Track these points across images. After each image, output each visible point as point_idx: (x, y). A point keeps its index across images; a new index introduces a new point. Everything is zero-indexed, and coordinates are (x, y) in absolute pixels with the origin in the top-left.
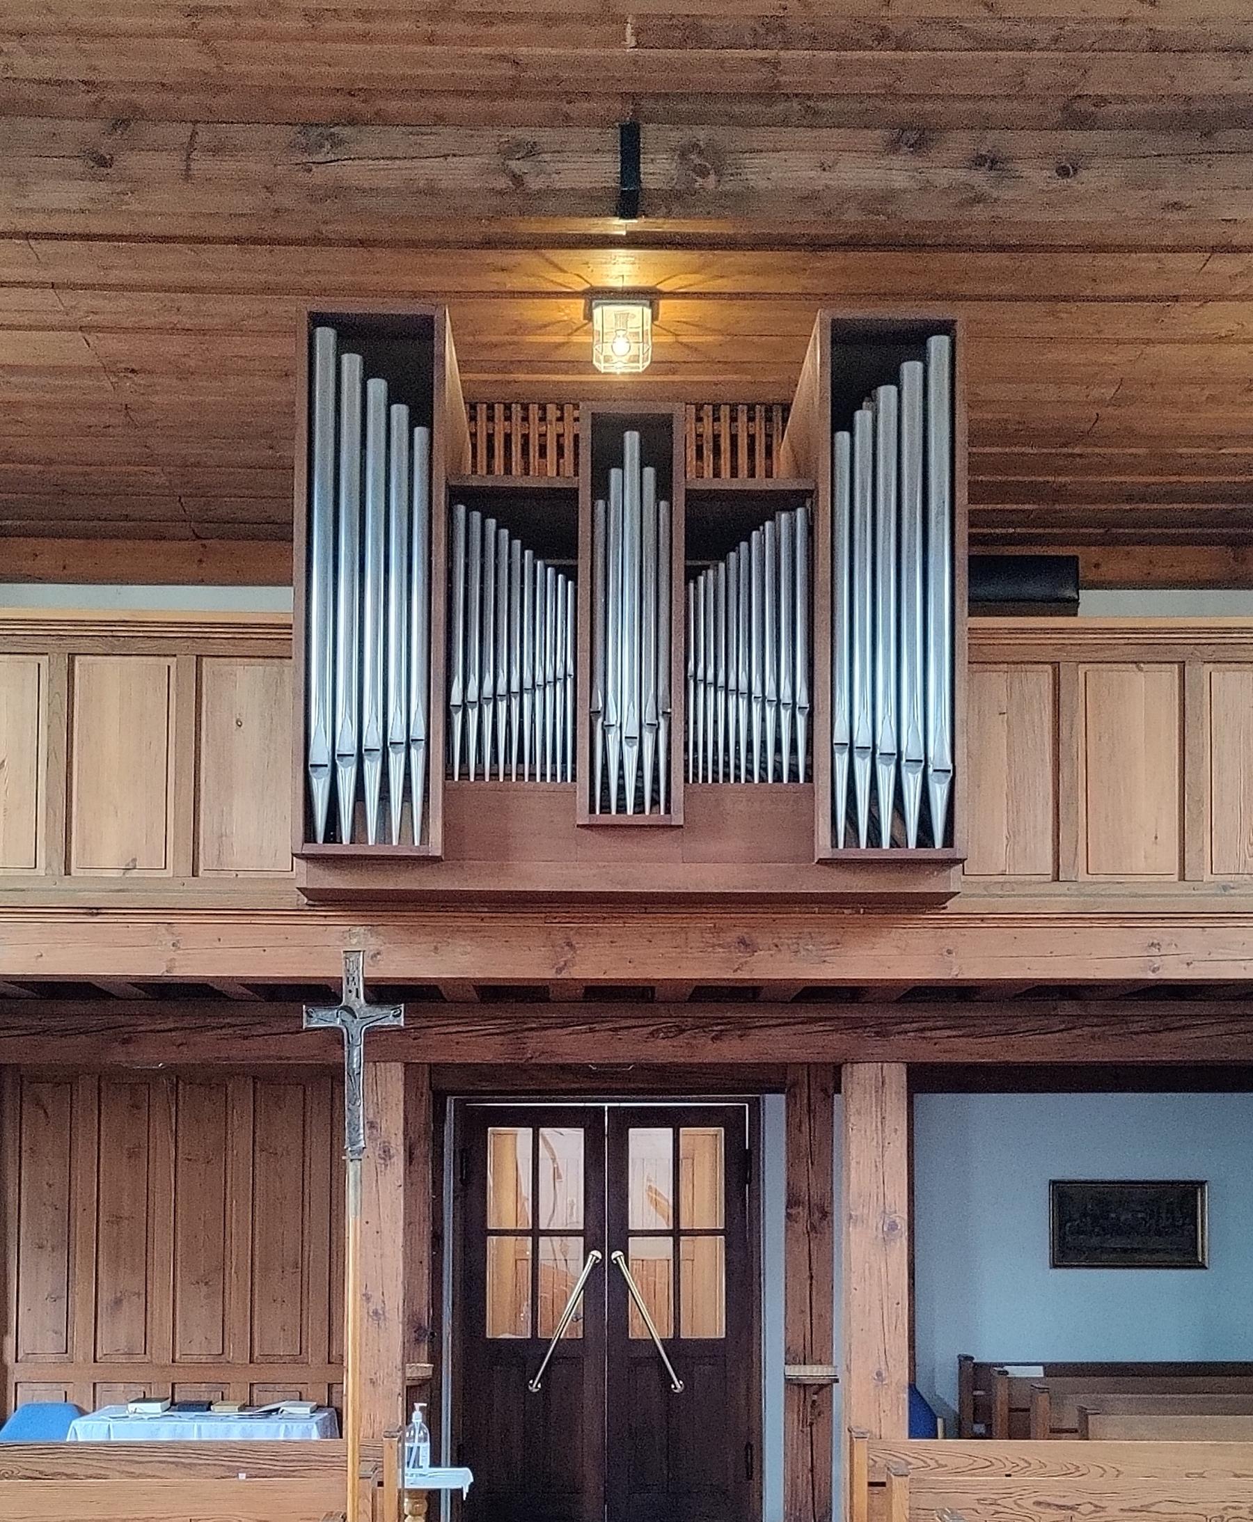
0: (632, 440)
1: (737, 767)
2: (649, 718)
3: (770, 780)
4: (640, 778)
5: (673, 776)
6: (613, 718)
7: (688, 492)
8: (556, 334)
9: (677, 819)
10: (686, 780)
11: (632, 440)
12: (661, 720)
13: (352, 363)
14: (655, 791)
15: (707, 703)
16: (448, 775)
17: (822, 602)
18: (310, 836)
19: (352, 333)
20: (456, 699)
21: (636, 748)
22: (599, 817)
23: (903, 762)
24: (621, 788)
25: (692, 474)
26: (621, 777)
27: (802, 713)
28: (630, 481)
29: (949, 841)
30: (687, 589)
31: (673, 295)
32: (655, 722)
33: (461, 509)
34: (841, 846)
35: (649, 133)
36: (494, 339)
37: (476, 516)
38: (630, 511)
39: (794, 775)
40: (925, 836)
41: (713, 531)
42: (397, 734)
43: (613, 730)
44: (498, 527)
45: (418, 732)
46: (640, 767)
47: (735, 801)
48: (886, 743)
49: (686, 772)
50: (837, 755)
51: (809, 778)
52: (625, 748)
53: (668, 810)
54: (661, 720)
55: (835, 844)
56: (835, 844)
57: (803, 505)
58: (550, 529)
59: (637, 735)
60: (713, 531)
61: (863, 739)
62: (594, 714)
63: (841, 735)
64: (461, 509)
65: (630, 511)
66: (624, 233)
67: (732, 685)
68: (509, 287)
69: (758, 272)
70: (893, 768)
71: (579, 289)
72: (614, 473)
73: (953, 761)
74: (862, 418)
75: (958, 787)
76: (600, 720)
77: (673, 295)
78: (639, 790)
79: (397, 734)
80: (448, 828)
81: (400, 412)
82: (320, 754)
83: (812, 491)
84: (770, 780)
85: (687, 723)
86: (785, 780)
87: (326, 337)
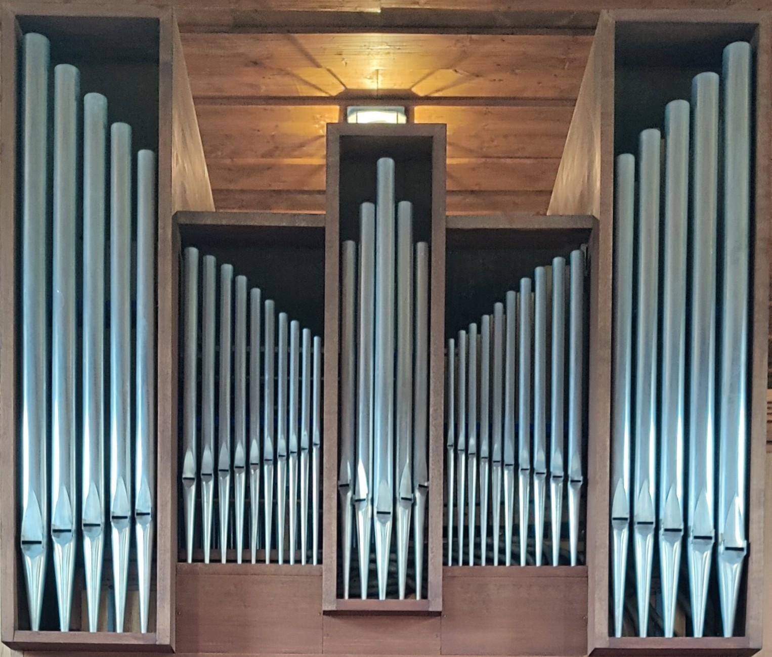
0: (386, 167)
1: (502, 551)
2: (403, 492)
3: (538, 563)
4: (393, 561)
5: (430, 555)
6: (363, 491)
7: (449, 231)
8: (311, 156)
9: (435, 605)
10: (445, 563)
11: (386, 167)
12: (418, 494)
13: (67, 74)
14: (410, 576)
15: (466, 472)
16: (181, 558)
17: (601, 352)
18: (23, 620)
19: (71, 43)
20: (189, 471)
21: (389, 524)
22: (347, 603)
23: (691, 539)
24: (373, 574)
25: (454, 213)
26: (373, 561)
27: (574, 487)
28: (384, 218)
29: (740, 628)
30: (447, 345)
31: (428, 100)
32: (410, 496)
33: (193, 252)
34: (618, 633)
35: (447, 189)
36: (251, 161)
37: (210, 260)
38: (384, 272)
39: (564, 559)
40: (713, 624)
41: (478, 275)
42: (120, 506)
43: (363, 504)
44: (236, 274)
45: (144, 503)
46: (393, 549)
47: (499, 586)
48: (671, 517)
49: (445, 555)
50: (615, 532)
51: (581, 561)
52: (378, 525)
53: (424, 596)
54: (418, 494)
55: (612, 632)
56: (612, 632)
57: (578, 248)
58: (287, 267)
59: (391, 510)
60: (478, 275)
61: (644, 512)
62: (342, 488)
63: (620, 509)
64: (193, 252)
65: (384, 272)
66: (379, 11)
67: (497, 456)
68: (263, 91)
69: (513, 66)
70: (677, 545)
71: (334, 93)
72: (366, 208)
73: (747, 536)
74: (650, 137)
75: (752, 567)
76: (349, 494)
77: (428, 100)
78: (392, 576)
79: (120, 506)
80: (180, 616)
81: (121, 131)
82: (33, 528)
83: (590, 230)
84: (538, 563)
85: (446, 505)
86: (555, 562)
87: (37, 45)
